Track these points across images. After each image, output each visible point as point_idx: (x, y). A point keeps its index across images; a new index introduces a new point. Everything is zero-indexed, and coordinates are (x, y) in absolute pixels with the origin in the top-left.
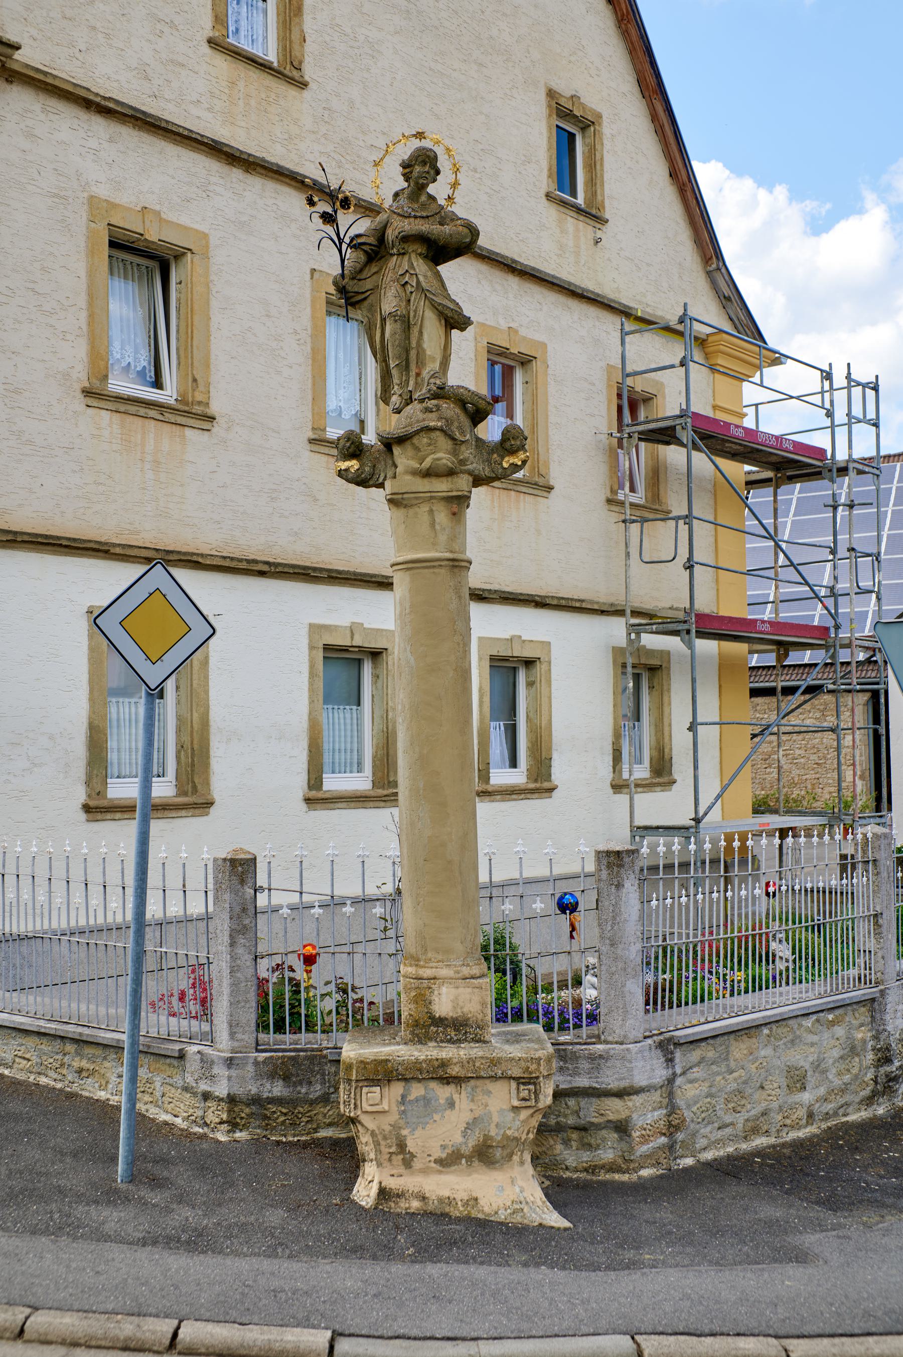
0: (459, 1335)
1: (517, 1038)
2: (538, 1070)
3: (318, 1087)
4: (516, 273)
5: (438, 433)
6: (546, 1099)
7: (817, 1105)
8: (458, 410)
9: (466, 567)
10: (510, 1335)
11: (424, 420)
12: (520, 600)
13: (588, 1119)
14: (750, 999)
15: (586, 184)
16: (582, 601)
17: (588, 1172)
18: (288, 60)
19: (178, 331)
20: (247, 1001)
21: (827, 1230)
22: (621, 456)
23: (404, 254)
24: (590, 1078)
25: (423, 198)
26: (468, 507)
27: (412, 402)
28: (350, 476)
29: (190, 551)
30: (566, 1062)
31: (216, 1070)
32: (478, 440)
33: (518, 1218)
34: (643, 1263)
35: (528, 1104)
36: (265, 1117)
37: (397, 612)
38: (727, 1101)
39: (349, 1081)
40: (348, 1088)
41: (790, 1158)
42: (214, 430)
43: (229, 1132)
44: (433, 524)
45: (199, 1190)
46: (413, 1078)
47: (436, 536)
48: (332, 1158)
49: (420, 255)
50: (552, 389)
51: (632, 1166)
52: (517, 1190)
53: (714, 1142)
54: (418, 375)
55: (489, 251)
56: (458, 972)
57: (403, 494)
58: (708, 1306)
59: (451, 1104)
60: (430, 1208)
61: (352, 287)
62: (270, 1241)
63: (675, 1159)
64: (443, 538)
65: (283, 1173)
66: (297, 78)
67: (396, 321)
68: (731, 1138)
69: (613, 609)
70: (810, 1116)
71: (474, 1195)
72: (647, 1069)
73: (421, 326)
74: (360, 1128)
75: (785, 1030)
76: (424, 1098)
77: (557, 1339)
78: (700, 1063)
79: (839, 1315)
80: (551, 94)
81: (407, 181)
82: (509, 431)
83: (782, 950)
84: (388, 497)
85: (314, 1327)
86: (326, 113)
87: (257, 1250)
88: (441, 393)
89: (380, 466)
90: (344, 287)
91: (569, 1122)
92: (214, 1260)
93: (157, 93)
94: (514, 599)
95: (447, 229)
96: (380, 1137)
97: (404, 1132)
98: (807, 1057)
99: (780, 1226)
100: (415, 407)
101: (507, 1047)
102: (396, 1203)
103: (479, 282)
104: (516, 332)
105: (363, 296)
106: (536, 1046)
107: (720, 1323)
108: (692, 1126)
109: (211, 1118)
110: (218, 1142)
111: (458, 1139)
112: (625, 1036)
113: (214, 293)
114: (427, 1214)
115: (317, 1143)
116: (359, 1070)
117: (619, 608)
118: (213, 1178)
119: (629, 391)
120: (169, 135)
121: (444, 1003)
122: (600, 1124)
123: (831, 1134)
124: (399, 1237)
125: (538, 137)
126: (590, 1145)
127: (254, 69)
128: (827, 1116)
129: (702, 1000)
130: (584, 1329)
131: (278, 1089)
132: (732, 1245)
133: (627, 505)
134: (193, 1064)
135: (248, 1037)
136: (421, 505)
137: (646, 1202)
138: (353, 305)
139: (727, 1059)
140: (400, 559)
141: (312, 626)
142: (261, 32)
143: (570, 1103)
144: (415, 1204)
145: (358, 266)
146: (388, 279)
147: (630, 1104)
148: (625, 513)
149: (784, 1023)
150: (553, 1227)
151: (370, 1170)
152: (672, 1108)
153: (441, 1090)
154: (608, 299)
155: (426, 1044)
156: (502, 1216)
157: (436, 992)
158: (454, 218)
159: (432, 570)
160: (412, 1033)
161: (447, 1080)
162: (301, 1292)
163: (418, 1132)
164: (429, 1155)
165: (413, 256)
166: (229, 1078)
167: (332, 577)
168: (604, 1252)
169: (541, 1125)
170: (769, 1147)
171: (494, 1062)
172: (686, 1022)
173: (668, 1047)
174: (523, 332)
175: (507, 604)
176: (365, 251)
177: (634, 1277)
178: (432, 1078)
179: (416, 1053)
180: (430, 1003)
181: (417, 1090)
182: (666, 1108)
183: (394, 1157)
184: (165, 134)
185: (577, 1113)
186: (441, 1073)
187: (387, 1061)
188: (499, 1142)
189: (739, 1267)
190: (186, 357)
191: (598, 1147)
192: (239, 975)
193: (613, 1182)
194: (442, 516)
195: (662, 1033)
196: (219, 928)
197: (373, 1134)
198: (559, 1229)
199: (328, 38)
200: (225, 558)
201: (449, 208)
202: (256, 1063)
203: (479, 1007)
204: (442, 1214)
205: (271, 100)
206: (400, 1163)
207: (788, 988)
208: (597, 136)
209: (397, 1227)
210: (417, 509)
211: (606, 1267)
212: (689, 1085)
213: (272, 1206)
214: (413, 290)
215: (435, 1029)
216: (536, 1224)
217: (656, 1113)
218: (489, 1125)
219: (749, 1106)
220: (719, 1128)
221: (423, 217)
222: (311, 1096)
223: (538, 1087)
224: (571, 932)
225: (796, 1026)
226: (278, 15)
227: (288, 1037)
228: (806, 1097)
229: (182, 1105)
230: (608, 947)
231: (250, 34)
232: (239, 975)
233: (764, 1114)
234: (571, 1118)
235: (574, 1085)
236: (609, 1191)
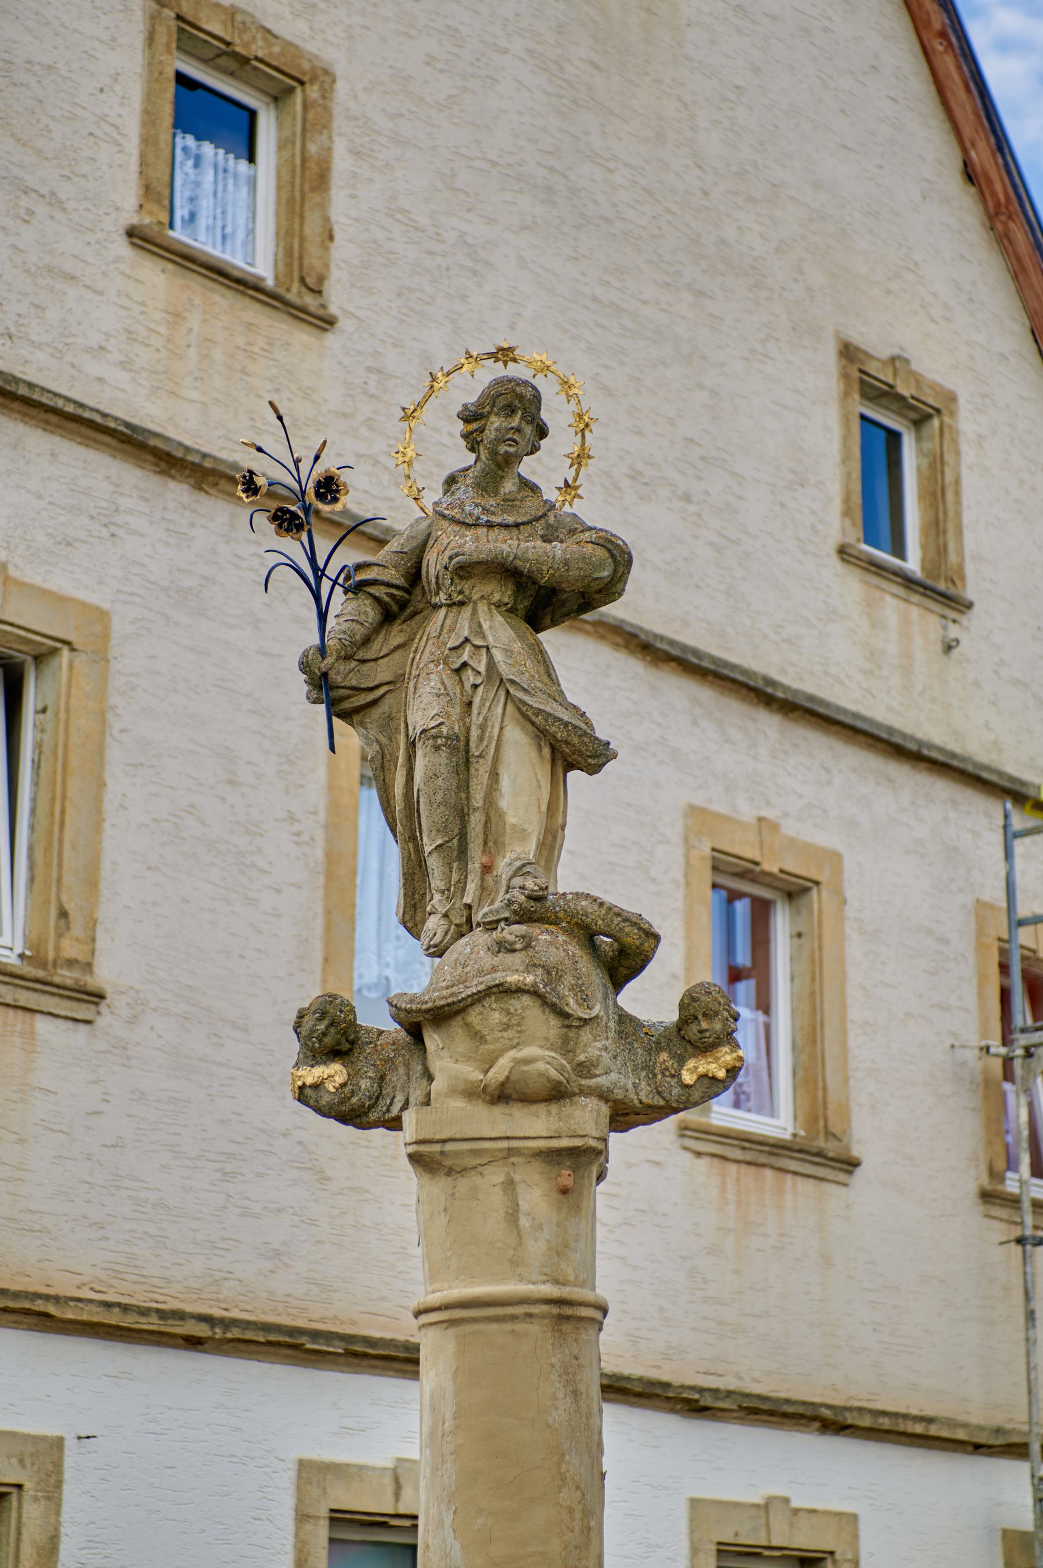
4: (775, 706)
5: (526, 1000)
8: (574, 949)
9: (592, 1320)
11: (494, 969)
12: (785, 1415)
15: (925, 531)
16: (929, 1420)
18: (296, 275)
19: (33, 811)
22: (1011, 1098)
23: (462, 604)
25: (509, 486)
26: (601, 1177)
27: (471, 929)
28: (325, 1100)
29: (31, 1289)
32: (624, 1018)
37: (426, 1429)
42: (102, 1022)
44: (513, 1215)
47: (520, 1243)
49: (498, 605)
50: (855, 949)
54: (487, 869)
55: (715, 660)
57: (444, 1141)
61: (342, 674)
64: (536, 1248)
66: (312, 309)
67: (437, 748)
69: (1000, 1441)
73: (496, 760)
80: (848, 352)
81: (472, 449)
82: (694, 1000)
84: (411, 1149)
86: (373, 379)
88: (535, 910)
89: (396, 1078)
90: (325, 675)
93: (13, 330)
94: (771, 1413)
95: (557, 549)
100: (480, 938)
103: (695, 723)
104: (775, 827)
105: (371, 697)
113: (115, 732)
117: (1015, 1439)
119: (1024, 958)
120: (34, 412)
125: (824, 439)
127: (223, 289)
133: (1026, 1205)
136: (487, 1170)
138: (346, 716)
140: (435, 1298)
141: (304, 1466)
142: (241, 220)
145: (360, 632)
146: (426, 657)
148: (1022, 1224)
154: (975, 764)
158: (576, 528)
159: (508, 1326)
165: (482, 608)
167: (355, 1354)
174: (790, 828)
175: (755, 1423)
176: (377, 599)
184: (25, 409)
190: (48, 865)
194: (535, 1195)
199: (380, 235)
200: (108, 1305)
201: (567, 508)
205: (256, 349)
208: (947, 435)
210: (477, 1180)
214: (479, 681)
221: (507, 526)
226: (279, 188)
231: (219, 223)
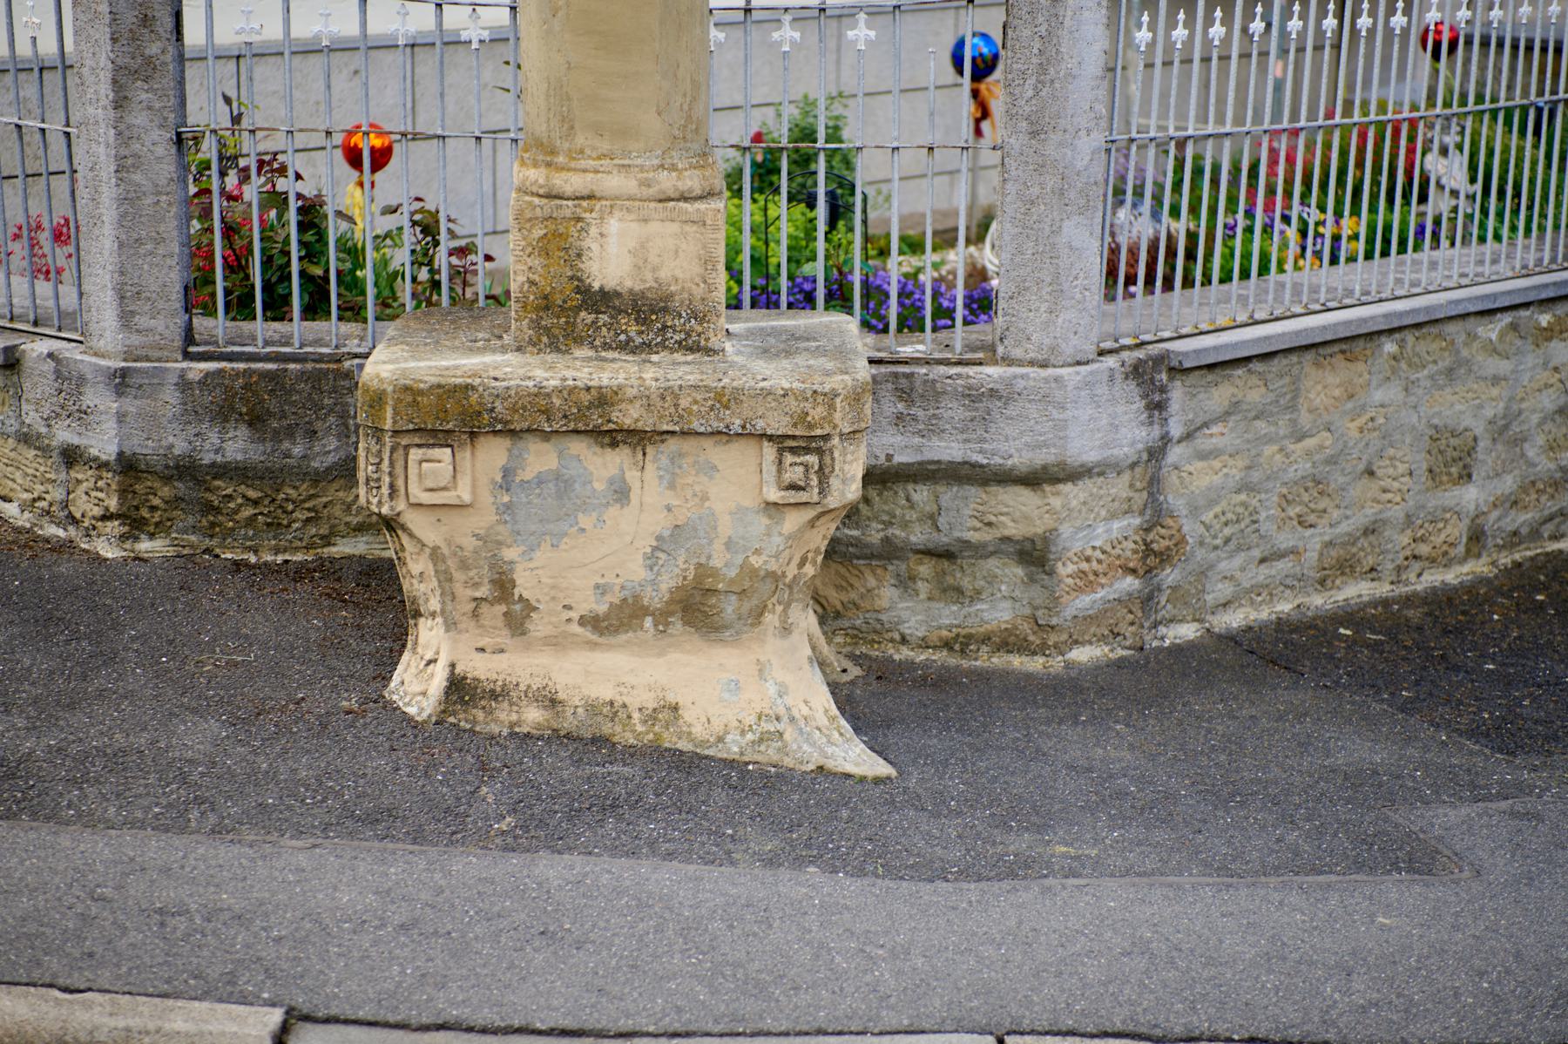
0: (588, 1026)
1: (790, 344)
2: (828, 419)
3: (332, 443)
6: (847, 487)
7: (1495, 514)
10: (711, 1027)
13: (957, 534)
14: (1357, 275)
17: (951, 649)
20: (159, 240)
21: (1488, 798)
24: (967, 441)
30: (910, 402)
31: (90, 398)
33: (769, 753)
34: (1049, 864)
35: (802, 497)
36: (209, 508)
38: (1286, 500)
39: (378, 432)
40: (374, 449)
41: (1420, 628)
43: (123, 538)
45: (29, 670)
46: (528, 430)
48: (357, 604)
51: (1052, 639)
52: (772, 690)
53: (1248, 591)
56: (646, 184)
58: (1189, 969)
59: (621, 493)
60: (568, 723)
62: (177, 793)
63: (1155, 625)
65: (237, 635)
68: (1288, 582)
70: (1477, 538)
71: (671, 698)
72: (1099, 422)
74: (405, 540)
75: (1435, 346)
76: (558, 477)
77: (821, 1038)
78: (1228, 413)
79: (1497, 999)
83: (1450, 171)
85: (244, 1000)
87: (139, 814)
91: (913, 539)
92: (32, 835)
96: (452, 564)
97: (510, 554)
98: (1481, 407)
99: (1380, 785)
101: (762, 367)
102: (489, 712)
106: (830, 365)
107: (1212, 1011)
108: (1200, 554)
109: (84, 505)
110: (99, 560)
111: (636, 571)
112: (1052, 349)
114: (560, 738)
115: (328, 569)
116: (401, 407)
118: (68, 642)
121: (614, 257)
122: (984, 545)
123: (1519, 580)
124: (485, 789)
126: (959, 590)
128: (1514, 539)
129: (1245, 274)
130: (890, 1019)
131: (237, 445)
132: (1263, 828)
134: (38, 383)
135: (166, 324)
137: (1076, 723)
139: (1292, 407)
143: (916, 497)
144: (533, 716)
147: (1056, 502)
149: (1434, 330)
150: (848, 776)
151: (429, 635)
152: (1156, 515)
153: (599, 460)
155: (567, 352)
156: (733, 747)
157: (593, 231)
160: (536, 325)
161: (612, 437)
162: (226, 915)
163: (542, 556)
164: (567, 607)
166: (121, 417)
168: (959, 837)
169: (834, 541)
170: (1375, 603)
171: (723, 399)
172: (1199, 320)
173: (1153, 375)
177: (1024, 896)
178: (576, 432)
179: (539, 373)
180: (579, 255)
181: (540, 458)
182: (1142, 513)
183: (485, 608)
185: (932, 518)
186: (596, 420)
187: (468, 387)
188: (732, 581)
189: (1273, 880)
191: (977, 595)
192: (137, 177)
193: (1006, 674)
195: (1143, 343)
196: (88, 62)
197: (435, 555)
198: (863, 779)
202: (184, 384)
203: (697, 269)
204: (594, 740)
206: (500, 622)
207: (1452, 251)
209: (483, 767)
211: (960, 872)
212: (1200, 464)
213: (194, 711)
215: (590, 318)
216: (811, 767)
217: (1116, 525)
218: (711, 542)
219: (1336, 514)
220: (1263, 561)
222: (315, 464)
223: (827, 460)
224: (978, 121)
225: (1461, 339)
227: (260, 328)
228: (1471, 496)
229: (18, 475)
230: (1024, 138)
232: (137, 177)
233: (1369, 531)
234: (917, 528)
235: (929, 455)
236: (995, 693)
